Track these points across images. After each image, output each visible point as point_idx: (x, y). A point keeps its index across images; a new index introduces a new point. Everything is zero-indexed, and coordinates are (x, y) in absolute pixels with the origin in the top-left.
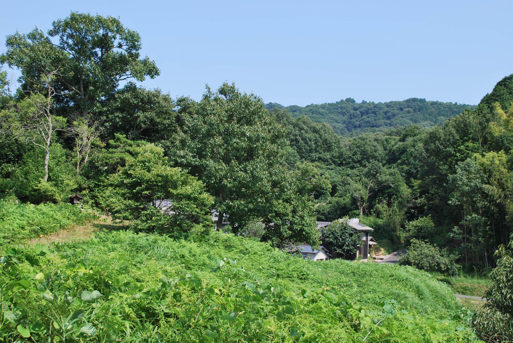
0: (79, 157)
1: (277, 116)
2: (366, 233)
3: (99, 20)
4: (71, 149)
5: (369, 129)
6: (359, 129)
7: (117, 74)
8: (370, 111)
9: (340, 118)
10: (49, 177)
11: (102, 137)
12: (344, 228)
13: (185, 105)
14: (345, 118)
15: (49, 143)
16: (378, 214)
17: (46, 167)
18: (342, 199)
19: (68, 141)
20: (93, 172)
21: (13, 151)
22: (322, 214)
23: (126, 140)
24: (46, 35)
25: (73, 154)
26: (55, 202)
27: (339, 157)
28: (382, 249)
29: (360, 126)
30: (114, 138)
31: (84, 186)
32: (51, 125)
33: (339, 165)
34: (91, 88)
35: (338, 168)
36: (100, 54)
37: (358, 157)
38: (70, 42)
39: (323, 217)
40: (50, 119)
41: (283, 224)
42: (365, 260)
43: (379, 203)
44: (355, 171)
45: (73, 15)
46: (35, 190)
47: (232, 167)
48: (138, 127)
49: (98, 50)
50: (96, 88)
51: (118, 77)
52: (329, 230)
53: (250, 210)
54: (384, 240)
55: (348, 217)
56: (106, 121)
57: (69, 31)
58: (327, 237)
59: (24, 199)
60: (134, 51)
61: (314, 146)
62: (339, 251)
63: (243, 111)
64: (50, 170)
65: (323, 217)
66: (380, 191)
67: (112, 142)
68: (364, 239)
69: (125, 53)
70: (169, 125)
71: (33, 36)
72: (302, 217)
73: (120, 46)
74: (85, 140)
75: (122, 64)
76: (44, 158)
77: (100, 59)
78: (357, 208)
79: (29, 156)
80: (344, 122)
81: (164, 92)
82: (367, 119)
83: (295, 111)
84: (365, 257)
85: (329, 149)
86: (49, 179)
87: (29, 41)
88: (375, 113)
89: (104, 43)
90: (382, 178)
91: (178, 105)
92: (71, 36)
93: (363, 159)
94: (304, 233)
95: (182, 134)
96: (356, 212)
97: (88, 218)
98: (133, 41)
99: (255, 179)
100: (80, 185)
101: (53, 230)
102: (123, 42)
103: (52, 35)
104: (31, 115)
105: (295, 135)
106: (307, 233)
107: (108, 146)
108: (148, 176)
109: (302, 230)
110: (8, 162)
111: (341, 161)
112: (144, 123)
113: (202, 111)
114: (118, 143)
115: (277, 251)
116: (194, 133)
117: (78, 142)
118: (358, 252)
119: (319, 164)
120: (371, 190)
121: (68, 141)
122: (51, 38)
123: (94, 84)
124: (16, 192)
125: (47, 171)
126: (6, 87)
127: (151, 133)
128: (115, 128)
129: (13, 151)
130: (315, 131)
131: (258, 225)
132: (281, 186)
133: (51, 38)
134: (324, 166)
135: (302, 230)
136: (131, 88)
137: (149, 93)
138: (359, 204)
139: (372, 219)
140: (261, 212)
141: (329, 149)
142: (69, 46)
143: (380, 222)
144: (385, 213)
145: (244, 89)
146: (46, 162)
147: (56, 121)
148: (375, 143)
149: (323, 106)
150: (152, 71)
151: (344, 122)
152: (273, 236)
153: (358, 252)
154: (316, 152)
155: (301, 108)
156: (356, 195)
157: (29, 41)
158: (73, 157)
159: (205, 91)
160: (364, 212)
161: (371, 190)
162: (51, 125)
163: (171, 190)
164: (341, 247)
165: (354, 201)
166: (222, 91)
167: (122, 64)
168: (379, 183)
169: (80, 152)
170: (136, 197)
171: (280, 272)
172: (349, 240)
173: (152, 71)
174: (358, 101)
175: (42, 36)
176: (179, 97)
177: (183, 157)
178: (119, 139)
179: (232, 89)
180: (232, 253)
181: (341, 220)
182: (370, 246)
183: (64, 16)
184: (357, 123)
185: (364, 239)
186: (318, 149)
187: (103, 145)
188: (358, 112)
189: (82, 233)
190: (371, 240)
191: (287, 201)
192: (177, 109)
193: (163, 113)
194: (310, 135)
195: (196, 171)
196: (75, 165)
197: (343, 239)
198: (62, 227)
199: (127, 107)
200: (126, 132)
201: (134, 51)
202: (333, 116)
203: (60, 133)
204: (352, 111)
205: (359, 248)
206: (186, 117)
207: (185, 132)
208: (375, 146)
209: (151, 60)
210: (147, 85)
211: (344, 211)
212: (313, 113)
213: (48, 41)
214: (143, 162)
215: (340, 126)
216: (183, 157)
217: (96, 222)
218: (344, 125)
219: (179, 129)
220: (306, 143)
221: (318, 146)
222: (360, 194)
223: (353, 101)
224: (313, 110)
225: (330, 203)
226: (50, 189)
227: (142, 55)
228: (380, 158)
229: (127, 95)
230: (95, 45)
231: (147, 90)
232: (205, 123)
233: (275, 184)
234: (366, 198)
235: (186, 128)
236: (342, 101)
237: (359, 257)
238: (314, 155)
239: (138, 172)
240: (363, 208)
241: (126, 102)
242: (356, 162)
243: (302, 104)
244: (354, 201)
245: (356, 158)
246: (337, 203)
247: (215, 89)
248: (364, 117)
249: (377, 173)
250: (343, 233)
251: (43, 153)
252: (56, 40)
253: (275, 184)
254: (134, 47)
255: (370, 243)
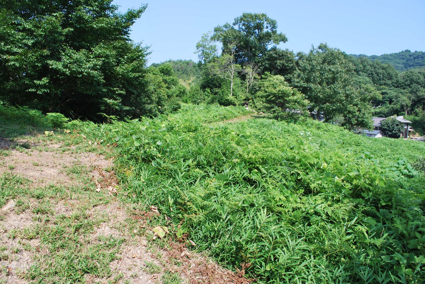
0: (248, 84)
1: (361, 61)
2: (407, 124)
3: (256, 16)
4: (244, 80)
5: (418, 67)
6: (412, 67)
7: (267, 42)
8: (419, 57)
9: (402, 61)
10: (233, 94)
11: (259, 74)
12: (394, 121)
13: (301, 56)
14: (404, 61)
15: (232, 77)
16: (417, 114)
17: (231, 89)
18: (395, 106)
19: (243, 77)
20: (253, 91)
21: (218, 82)
22: (383, 114)
23: (270, 75)
24: (232, 25)
25: (245, 82)
26: (235, 105)
27: (396, 83)
28: (417, 134)
29: (413, 65)
30: (264, 74)
31: (250, 98)
32: (233, 69)
33: (396, 87)
34: (254, 49)
35: (395, 89)
36: (257, 33)
37: (408, 82)
38: (243, 27)
39: (384, 116)
40: (232, 66)
41: (353, 117)
42: (406, 139)
43: (417, 108)
44: (406, 90)
45: (244, 14)
46: (227, 100)
47: (323, 87)
48: (277, 69)
49: (257, 31)
50: (256, 49)
51: (267, 43)
52: (385, 122)
53: (333, 110)
54: (419, 129)
55: (396, 115)
56: (261, 66)
57: (243, 22)
58: (383, 126)
59: (221, 104)
60: (274, 30)
61: (382, 77)
62: (390, 133)
63: (330, 57)
64: (233, 90)
65: (384, 116)
66: (418, 101)
67: (263, 76)
68: (406, 127)
69: (270, 31)
70: (292, 67)
71: (226, 26)
72: (364, 114)
73: (267, 27)
74: (251, 76)
75: (268, 36)
76: (230, 85)
77: (258, 35)
78: (404, 111)
79: (224, 84)
80: (403, 63)
81: (290, 50)
82: (418, 61)
83: (374, 58)
84: (406, 137)
85: (391, 78)
86: (233, 95)
87: (224, 29)
88: (422, 58)
89: (259, 27)
90: (420, 94)
91: (297, 56)
92: (244, 25)
93: (411, 83)
94: (364, 122)
95: (299, 71)
96: (403, 113)
97: (249, 113)
98: (273, 24)
99: (336, 93)
100: (248, 98)
101: (231, 118)
102: (269, 25)
103: (234, 25)
104: (224, 64)
105: (371, 71)
106: (366, 122)
107: (262, 78)
108: (274, 91)
109: (363, 121)
110: (216, 88)
111: (398, 85)
112: (279, 66)
113: (309, 59)
114: (266, 77)
115: (346, 131)
116: (304, 70)
117: (247, 77)
118: (401, 135)
119: (384, 87)
120: (413, 100)
121: (243, 77)
122: (234, 26)
123: (255, 48)
124: (219, 101)
125: (232, 91)
126: (216, 52)
127: (283, 71)
128: (266, 69)
129: (218, 82)
130: (383, 69)
131: (341, 118)
132: (351, 97)
133: (234, 26)
134: (387, 88)
135: (363, 121)
136: (274, 49)
137: (283, 51)
138: (405, 108)
139: (412, 117)
140: (340, 111)
141: (391, 78)
142: (243, 30)
143: (417, 118)
144: (421, 113)
145: (332, 45)
146: (231, 87)
147: (236, 67)
148: (419, 75)
149: (391, 55)
150: (284, 40)
151: (403, 63)
152: (348, 124)
153: (401, 135)
154: (383, 80)
155: (378, 56)
156: (404, 103)
157: (224, 29)
158: (245, 84)
159: (310, 48)
160: (408, 113)
161: (413, 100)
162: (233, 69)
163: (286, 98)
164: (391, 131)
165: (402, 107)
166: (320, 48)
167: (268, 36)
168: (418, 97)
169: (249, 82)
170: (269, 102)
171: (345, 141)
172: (396, 128)
173: (284, 40)
174: (413, 51)
175: (230, 26)
176: (298, 52)
177: (298, 82)
178: (266, 75)
179: (325, 46)
180: (320, 131)
181: (392, 117)
182: (410, 132)
183: (240, 15)
184: (411, 64)
185: (406, 127)
186: (384, 79)
187: (260, 78)
188: (412, 58)
189: (245, 119)
190: (411, 128)
191: (356, 105)
192: (297, 58)
193: (289, 60)
194: (381, 71)
195: (304, 90)
196: (246, 88)
197: (392, 127)
198: (236, 117)
199: (271, 59)
200: (271, 71)
201: (274, 30)
202: (397, 60)
203: (239, 73)
204: (408, 57)
205: (402, 132)
206: (300, 62)
207: (300, 70)
208: (418, 76)
209: (283, 34)
210: (282, 46)
211: (397, 112)
212: (385, 59)
213: (233, 28)
214: (273, 85)
215: (401, 65)
216: (298, 82)
217: (252, 115)
218: (403, 65)
219: (297, 68)
220: (378, 75)
221: (384, 77)
222: (406, 103)
223: (409, 51)
224: (385, 57)
225: (388, 108)
226: (233, 99)
227: (278, 32)
228: (421, 83)
229: (271, 52)
230: (255, 28)
231: (281, 49)
232: (310, 65)
233: (347, 96)
234: (409, 105)
235: (300, 68)
236: (403, 51)
237: (402, 137)
238: (382, 82)
239: (271, 90)
240: (408, 111)
241: (271, 56)
242: (407, 86)
243: (379, 54)
244: (402, 107)
245: (407, 83)
246: (392, 108)
247: (316, 47)
248: (416, 60)
249: (417, 91)
250: (393, 124)
251: (230, 82)
252: (236, 27)
253: (347, 96)
254: (274, 27)
255: (410, 130)
